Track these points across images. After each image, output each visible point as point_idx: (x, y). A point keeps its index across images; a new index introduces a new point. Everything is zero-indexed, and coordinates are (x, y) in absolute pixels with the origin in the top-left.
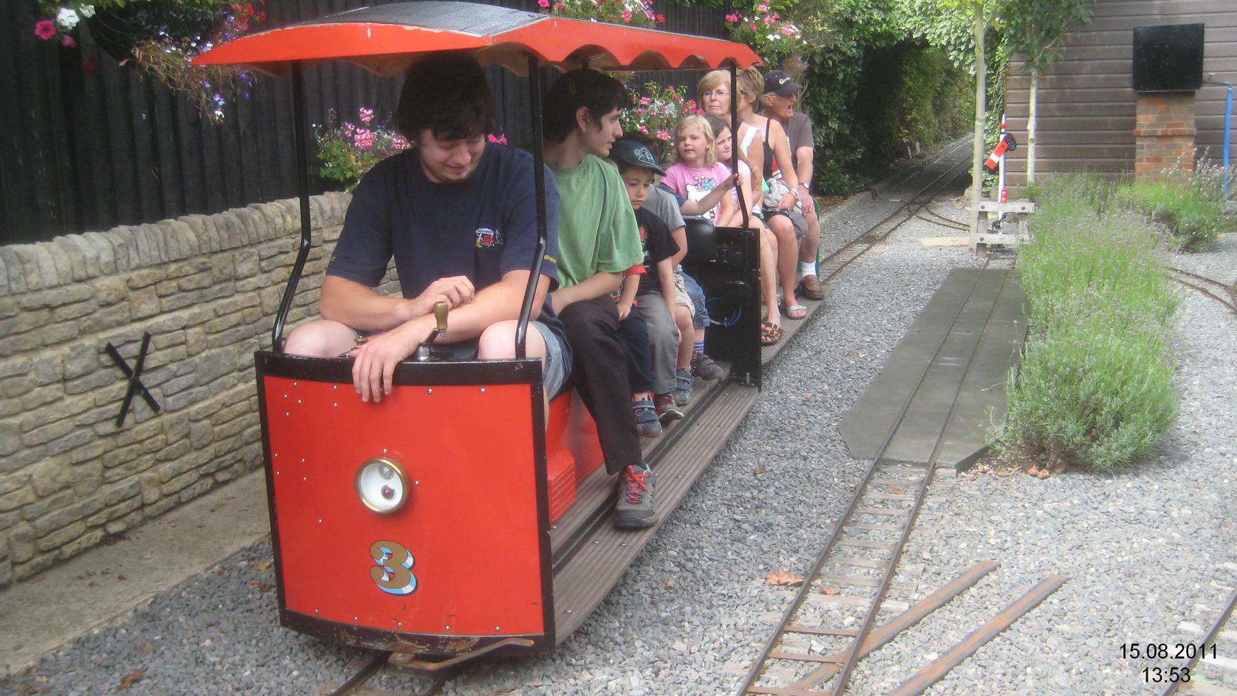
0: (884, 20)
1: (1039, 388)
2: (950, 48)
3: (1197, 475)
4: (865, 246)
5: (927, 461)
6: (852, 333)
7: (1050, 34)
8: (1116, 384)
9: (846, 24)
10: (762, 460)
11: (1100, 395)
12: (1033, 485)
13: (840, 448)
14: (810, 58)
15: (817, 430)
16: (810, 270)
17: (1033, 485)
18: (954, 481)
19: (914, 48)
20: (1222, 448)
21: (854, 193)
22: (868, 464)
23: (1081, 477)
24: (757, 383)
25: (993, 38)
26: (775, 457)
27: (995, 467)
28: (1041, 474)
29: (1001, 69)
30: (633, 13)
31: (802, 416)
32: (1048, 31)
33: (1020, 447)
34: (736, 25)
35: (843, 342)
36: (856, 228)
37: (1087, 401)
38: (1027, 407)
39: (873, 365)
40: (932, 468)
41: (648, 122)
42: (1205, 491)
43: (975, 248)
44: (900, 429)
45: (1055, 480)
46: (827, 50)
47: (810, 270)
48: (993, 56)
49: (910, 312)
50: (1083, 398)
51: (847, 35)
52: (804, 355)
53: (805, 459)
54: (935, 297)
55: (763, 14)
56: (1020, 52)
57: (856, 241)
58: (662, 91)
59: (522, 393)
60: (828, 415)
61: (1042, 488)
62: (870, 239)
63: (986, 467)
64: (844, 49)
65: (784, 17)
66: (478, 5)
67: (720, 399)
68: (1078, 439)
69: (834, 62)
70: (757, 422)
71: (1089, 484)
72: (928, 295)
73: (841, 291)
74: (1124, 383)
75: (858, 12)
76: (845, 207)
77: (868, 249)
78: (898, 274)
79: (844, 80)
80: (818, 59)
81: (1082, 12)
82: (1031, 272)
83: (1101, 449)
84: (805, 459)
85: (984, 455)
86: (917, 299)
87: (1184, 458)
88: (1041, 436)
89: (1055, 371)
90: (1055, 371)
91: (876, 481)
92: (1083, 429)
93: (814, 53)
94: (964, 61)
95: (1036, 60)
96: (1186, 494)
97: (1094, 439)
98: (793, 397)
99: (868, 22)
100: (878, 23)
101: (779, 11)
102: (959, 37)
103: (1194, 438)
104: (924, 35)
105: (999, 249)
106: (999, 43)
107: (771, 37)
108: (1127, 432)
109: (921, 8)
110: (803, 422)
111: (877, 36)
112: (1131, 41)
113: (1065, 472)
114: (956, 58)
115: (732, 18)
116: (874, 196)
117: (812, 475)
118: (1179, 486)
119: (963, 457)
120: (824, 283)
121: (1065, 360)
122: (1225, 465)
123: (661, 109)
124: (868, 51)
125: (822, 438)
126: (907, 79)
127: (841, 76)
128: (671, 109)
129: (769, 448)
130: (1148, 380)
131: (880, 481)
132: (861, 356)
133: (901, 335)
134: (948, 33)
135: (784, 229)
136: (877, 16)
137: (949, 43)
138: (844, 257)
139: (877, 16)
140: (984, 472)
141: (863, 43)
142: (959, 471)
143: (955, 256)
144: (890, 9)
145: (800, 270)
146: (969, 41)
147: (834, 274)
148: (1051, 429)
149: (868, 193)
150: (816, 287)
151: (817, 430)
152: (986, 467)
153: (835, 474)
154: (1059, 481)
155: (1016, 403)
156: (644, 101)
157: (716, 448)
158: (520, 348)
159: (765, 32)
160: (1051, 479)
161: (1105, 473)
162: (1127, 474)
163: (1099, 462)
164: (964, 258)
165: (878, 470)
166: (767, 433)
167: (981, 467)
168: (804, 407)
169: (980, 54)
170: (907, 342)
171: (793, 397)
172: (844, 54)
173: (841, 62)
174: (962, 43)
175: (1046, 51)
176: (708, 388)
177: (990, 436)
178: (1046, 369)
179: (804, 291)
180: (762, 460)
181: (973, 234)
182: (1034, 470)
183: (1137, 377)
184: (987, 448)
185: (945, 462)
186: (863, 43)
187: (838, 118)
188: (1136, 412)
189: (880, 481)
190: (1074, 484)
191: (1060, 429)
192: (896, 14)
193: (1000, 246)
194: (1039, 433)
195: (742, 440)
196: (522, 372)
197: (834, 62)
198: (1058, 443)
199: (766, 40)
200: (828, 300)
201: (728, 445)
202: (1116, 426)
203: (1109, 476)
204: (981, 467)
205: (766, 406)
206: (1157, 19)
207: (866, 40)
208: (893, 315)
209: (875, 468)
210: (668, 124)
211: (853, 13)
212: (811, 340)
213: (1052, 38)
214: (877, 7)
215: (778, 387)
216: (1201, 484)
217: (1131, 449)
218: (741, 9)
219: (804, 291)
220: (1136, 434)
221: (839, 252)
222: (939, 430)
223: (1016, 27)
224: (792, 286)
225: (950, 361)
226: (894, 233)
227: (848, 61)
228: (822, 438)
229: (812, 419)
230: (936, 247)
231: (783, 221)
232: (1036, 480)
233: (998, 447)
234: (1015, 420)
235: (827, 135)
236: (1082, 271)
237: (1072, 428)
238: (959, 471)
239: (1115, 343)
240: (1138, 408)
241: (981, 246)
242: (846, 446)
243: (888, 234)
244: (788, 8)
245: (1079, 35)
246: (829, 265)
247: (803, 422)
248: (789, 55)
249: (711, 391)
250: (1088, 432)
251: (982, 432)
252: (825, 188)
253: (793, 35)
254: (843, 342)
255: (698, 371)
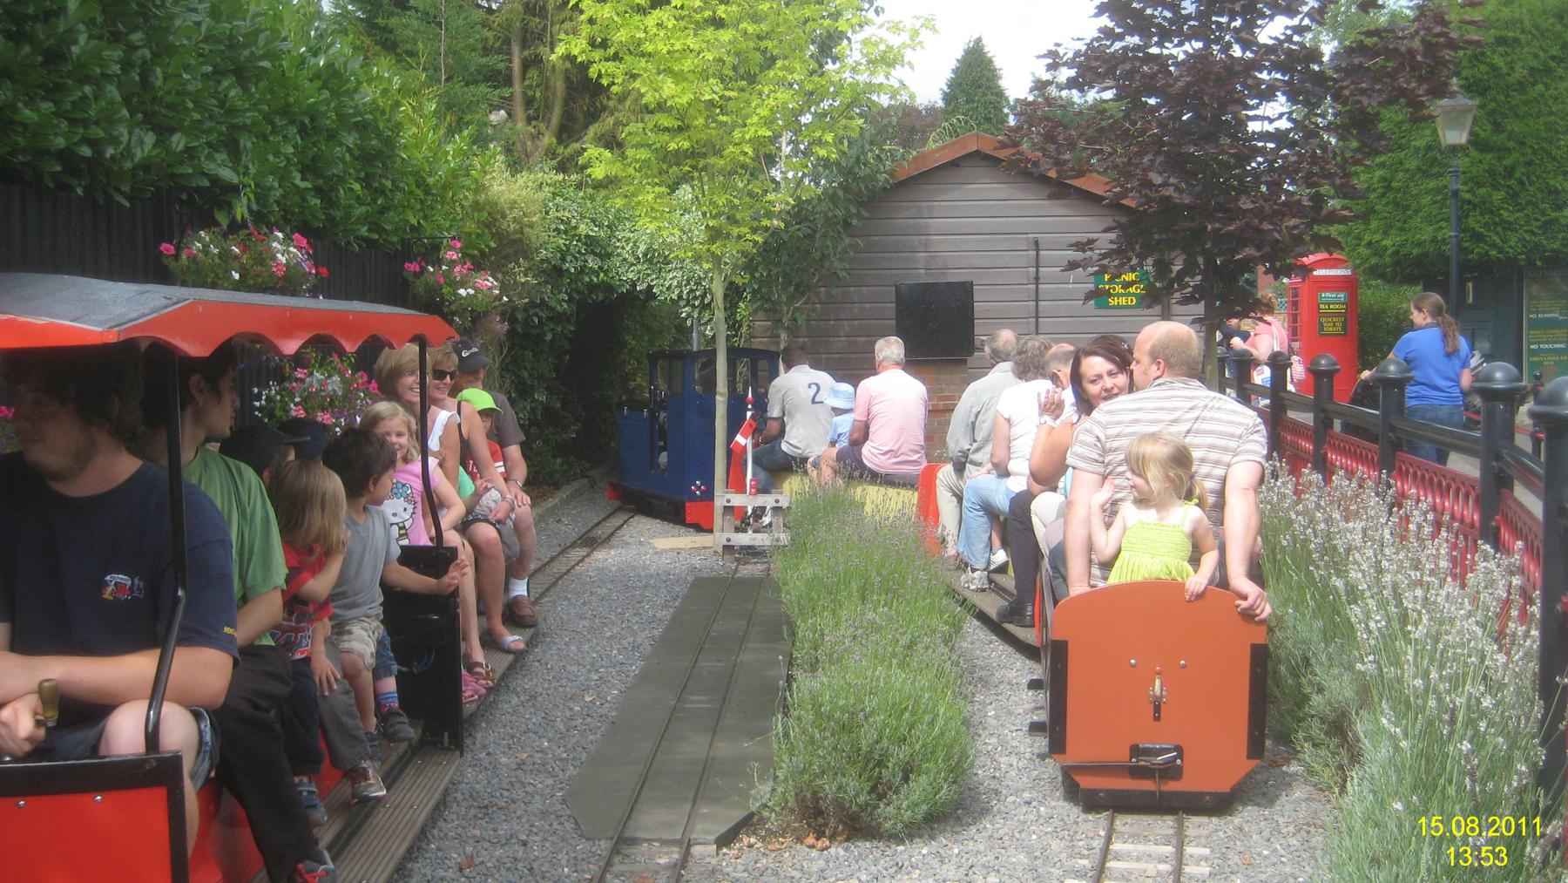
0: (601, 268)
1: (812, 738)
2: (682, 303)
3: (1001, 832)
4: (582, 552)
5: (679, 836)
6: (575, 669)
7: (801, 289)
8: (904, 730)
9: (554, 273)
10: (469, 849)
11: (885, 743)
12: (811, 860)
13: (569, 826)
14: (509, 315)
15: (537, 804)
16: (520, 589)
17: (811, 860)
18: (714, 861)
19: (637, 302)
20: (1026, 795)
21: (568, 481)
22: (604, 846)
23: (868, 844)
24: (458, 745)
25: (733, 293)
26: (486, 845)
27: (763, 839)
28: (820, 844)
29: (744, 330)
30: (287, 265)
31: (518, 785)
32: (798, 287)
33: (792, 811)
34: (417, 275)
35: (564, 682)
36: (569, 529)
37: (871, 752)
38: (800, 760)
39: (603, 711)
40: (687, 846)
41: (305, 400)
42: (1012, 851)
43: (720, 550)
44: (643, 794)
45: (838, 851)
46: (532, 304)
47: (520, 589)
48: (734, 314)
49: (645, 638)
50: (864, 748)
51: (557, 287)
52: (515, 701)
53: (525, 844)
54: (674, 619)
55: (452, 263)
56: (766, 311)
57: (573, 545)
58: (323, 359)
59: (152, 802)
60: (550, 782)
61: (822, 863)
62: (590, 541)
63: (753, 840)
64: (553, 304)
65: (478, 267)
66: (95, 281)
67: (411, 770)
68: (862, 799)
69: (540, 319)
70: (459, 796)
71: (877, 853)
72: (666, 614)
73: (556, 612)
74: (911, 727)
75: (569, 258)
76: (557, 500)
77: (588, 555)
78: (629, 584)
79: (553, 340)
80: (520, 316)
81: (836, 264)
82: (795, 581)
83: (890, 809)
84: (525, 844)
85: (748, 824)
86: (653, 620)
87: (986, 811)
88: (816, 797)
89: (830, 718)
90: (830, 718)
91: (617, 868)
92: (867, 786)
93: (515, 309)
94: (699, 319)
95: (785, 319)
96: (991, 858)
97: (881, 797)
98: (504, 760)
99: (582, 270)
100: (592, 271)
101: (472, 256)
102: (692, 291)
103: (994, 785)
104: (650, 287)
105: (751, 552)
106: (740, 298)
107: (462, 292)
108: (919, 786)
109: (645, 255)
110: (519, 794)
111: (592, 287)
112: (893, 298)
113: (848, 840)
114: (689, 315)
115: (412, 267)
116: (593, 484)
117: (535, 865)
118: (981, 847)
119: (723, 829)
120: (535, 603)
121: (841, 703)
122: (1032, 817)
123: (323, 384)
124: (582, 306)
125: (545, 814)
126: (628, 338)
127: (549, 337)
128: (335, 384)
129: (477, 832)
130: (940, 722)
131: (622, 868)
132: (588, 699)
133: (635, 669)
134: (679, 286)
135: (488, 541)
136: (592, 263)
137: (680, 297)
138: (560, 567)
139: (592, 263)
140: (750, 846)
141: (576, 296)
142: (719, 848)
143: (696, 561)
144: (609, 256)
145: (507, 589)
146: (704, 296)
147: (548, 590)
148: (829, 789)
149: (585, 481)
150: (527, 611)
151: (537, 804)
152: (753, 840)
153: (564, 862)
154: (842, 852)
155: (786, 757)
156: (300, 374)
157: (410, 838)
158: (152, 736)
159: (456, 285)
160: (832, 850)
161: (895, 838)
162: (921, 837)
163: (888, 825)
164: (707, 563)
165: (618, 853)
166: (473, 812)
167: (746, 841)
168: (519, 773)
169: (720, 315)
170: (645, 677)
171: (504, 760)
172: (553, 309)
173: (549, 319)
174: (696, 298)
175: (796, 310)
176: (394, 756)
177: (756, 799)
178: (819, 714)
179: (514, 616)
180: (469, 849)
181: (717, 534)
182: (810, 840)
183: (927, 718)
184: (752, 815)
185: (702, 837)
186: (576, 296)
187: (547, 388)
188: (928, 761)
189: (622, 868)
190: (860, 854)
191: (840, 788)
192: (616, 261)
193: (750, 547)
194: (815, 793)
195: (441, 824)
196: (156, 770)
197: (540, 319)
198: (839, 805)
199: (456, 294)
200: (543, 627)
201: (423, 833)
202: (906, 779)
203: (901, 841)
204: (746, 841)
205: (470, 774)
206: (922, 276)
207: (578, 292)
208: (625, 643)
209: (615, 851)
210: (332, 403)
211: (563, 260)
212: (524, 683)
213: (803, 293)
214: (593, 252)
215: (484, 747)
216: (1007, 843)
217: (924, 807)
218: (424, 255)
219: (514, 616)
220: (929, 788)
221: (552, 559)
222: (692, 795)
223: (760, 282)
224: (497, 611)
225: (699, 701)
226: (620, 533)
227: (558, 318)
228: (545, 814)
229: (530, 789)
230: (671, 550)
231: (486, 532)
232: (814, 853)
233: (766, 814)
234: (786, 780)
235: (533, 410)
236: (854, 586)
237: (854, 787)
238: (719, 848)
239: (899, 677)
240: (929, 754)
241: (728, 548)
242: (577, 823)
243: (612, 534)
244: (482, 252)
245: (834, 291)
246: (540, 578)
247: (519, 794)
248: (486, 314)
249: (400, 758)
250: (873, 789)
251: (745, 795)
252: (537, 484)
253: (490, 289)
254: (564, 682)
255: (387, 735)
